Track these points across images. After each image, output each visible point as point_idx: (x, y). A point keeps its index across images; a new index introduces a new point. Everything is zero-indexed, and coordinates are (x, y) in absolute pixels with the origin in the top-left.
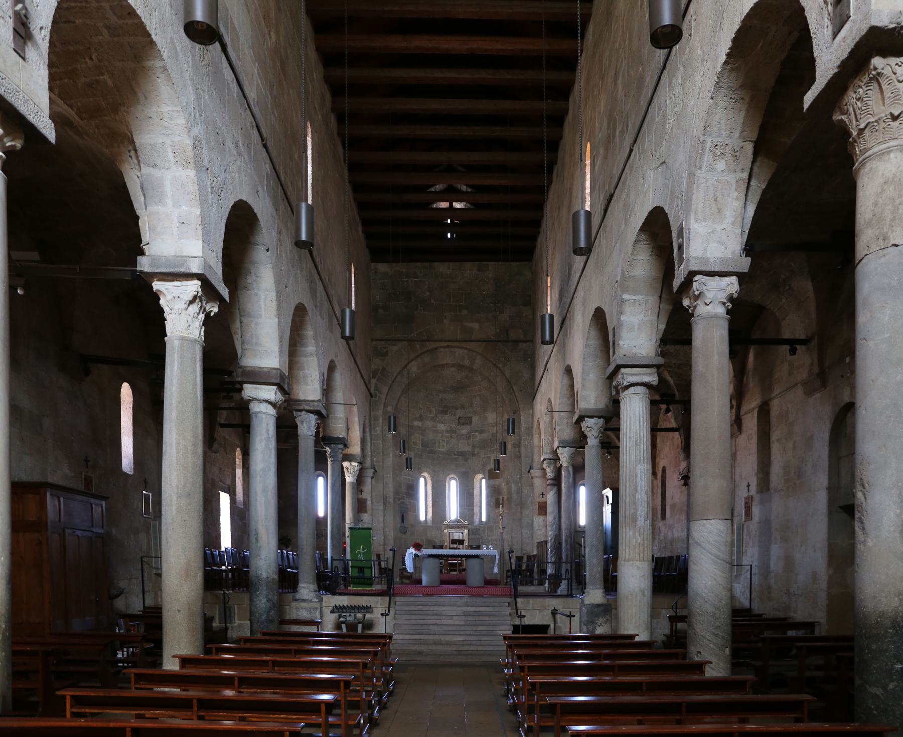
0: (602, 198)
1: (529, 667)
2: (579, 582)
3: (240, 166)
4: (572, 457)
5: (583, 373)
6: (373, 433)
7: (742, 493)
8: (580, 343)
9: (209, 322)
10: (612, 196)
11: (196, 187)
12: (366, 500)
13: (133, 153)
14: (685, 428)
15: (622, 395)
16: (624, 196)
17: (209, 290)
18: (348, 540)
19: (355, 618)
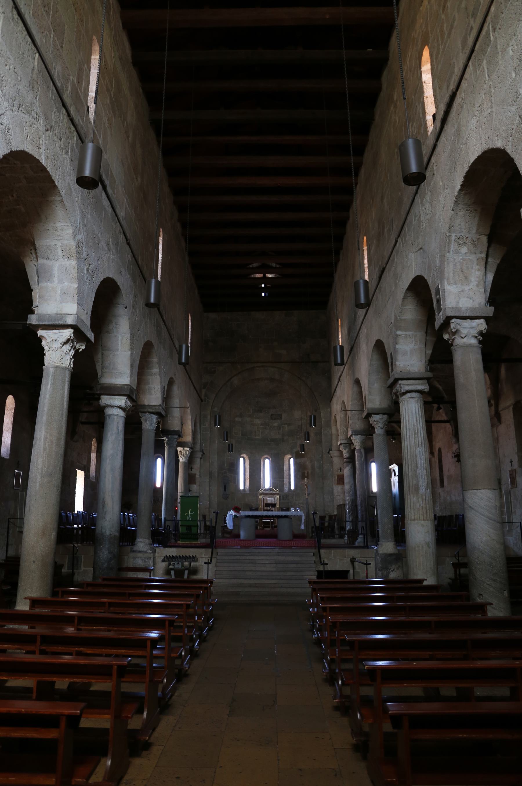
0: (377, 270)
1: (330, 608)
2: (373, 535)
3: (109, 257)
4: (363, 443)
5: (369, 384)
6: (202, 426)
7: (506, 468)
8: (365, 364)
9: (77, 356)
10: (384, 269)
11: (76, 271)
12: (195, 474)
13: (33, 251)
14: (453, 419)
15: (401, 399)
16: (393, 269)
17: (79, 334)
18: (179, 505)
19: (183, 565)
